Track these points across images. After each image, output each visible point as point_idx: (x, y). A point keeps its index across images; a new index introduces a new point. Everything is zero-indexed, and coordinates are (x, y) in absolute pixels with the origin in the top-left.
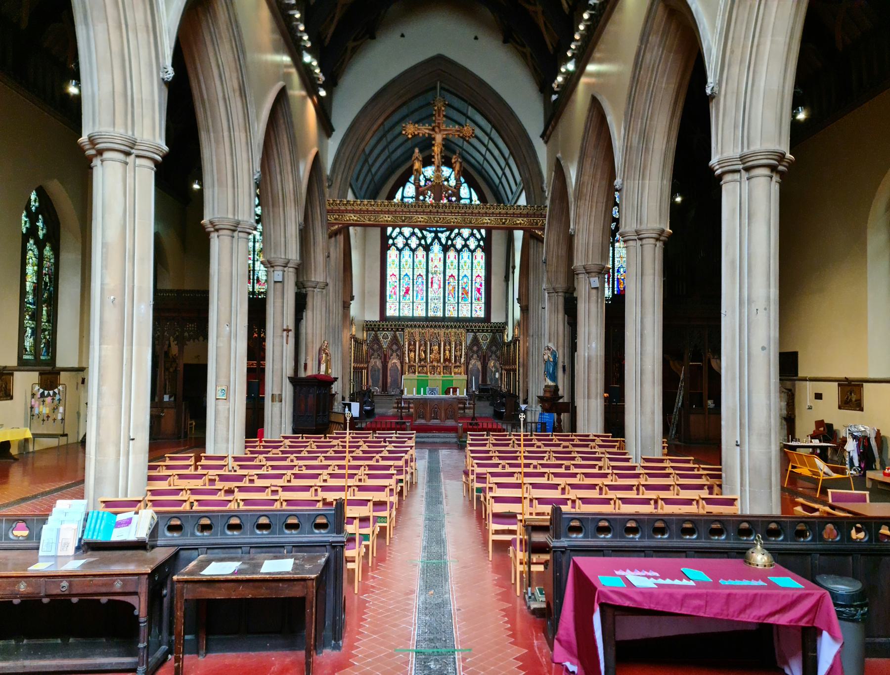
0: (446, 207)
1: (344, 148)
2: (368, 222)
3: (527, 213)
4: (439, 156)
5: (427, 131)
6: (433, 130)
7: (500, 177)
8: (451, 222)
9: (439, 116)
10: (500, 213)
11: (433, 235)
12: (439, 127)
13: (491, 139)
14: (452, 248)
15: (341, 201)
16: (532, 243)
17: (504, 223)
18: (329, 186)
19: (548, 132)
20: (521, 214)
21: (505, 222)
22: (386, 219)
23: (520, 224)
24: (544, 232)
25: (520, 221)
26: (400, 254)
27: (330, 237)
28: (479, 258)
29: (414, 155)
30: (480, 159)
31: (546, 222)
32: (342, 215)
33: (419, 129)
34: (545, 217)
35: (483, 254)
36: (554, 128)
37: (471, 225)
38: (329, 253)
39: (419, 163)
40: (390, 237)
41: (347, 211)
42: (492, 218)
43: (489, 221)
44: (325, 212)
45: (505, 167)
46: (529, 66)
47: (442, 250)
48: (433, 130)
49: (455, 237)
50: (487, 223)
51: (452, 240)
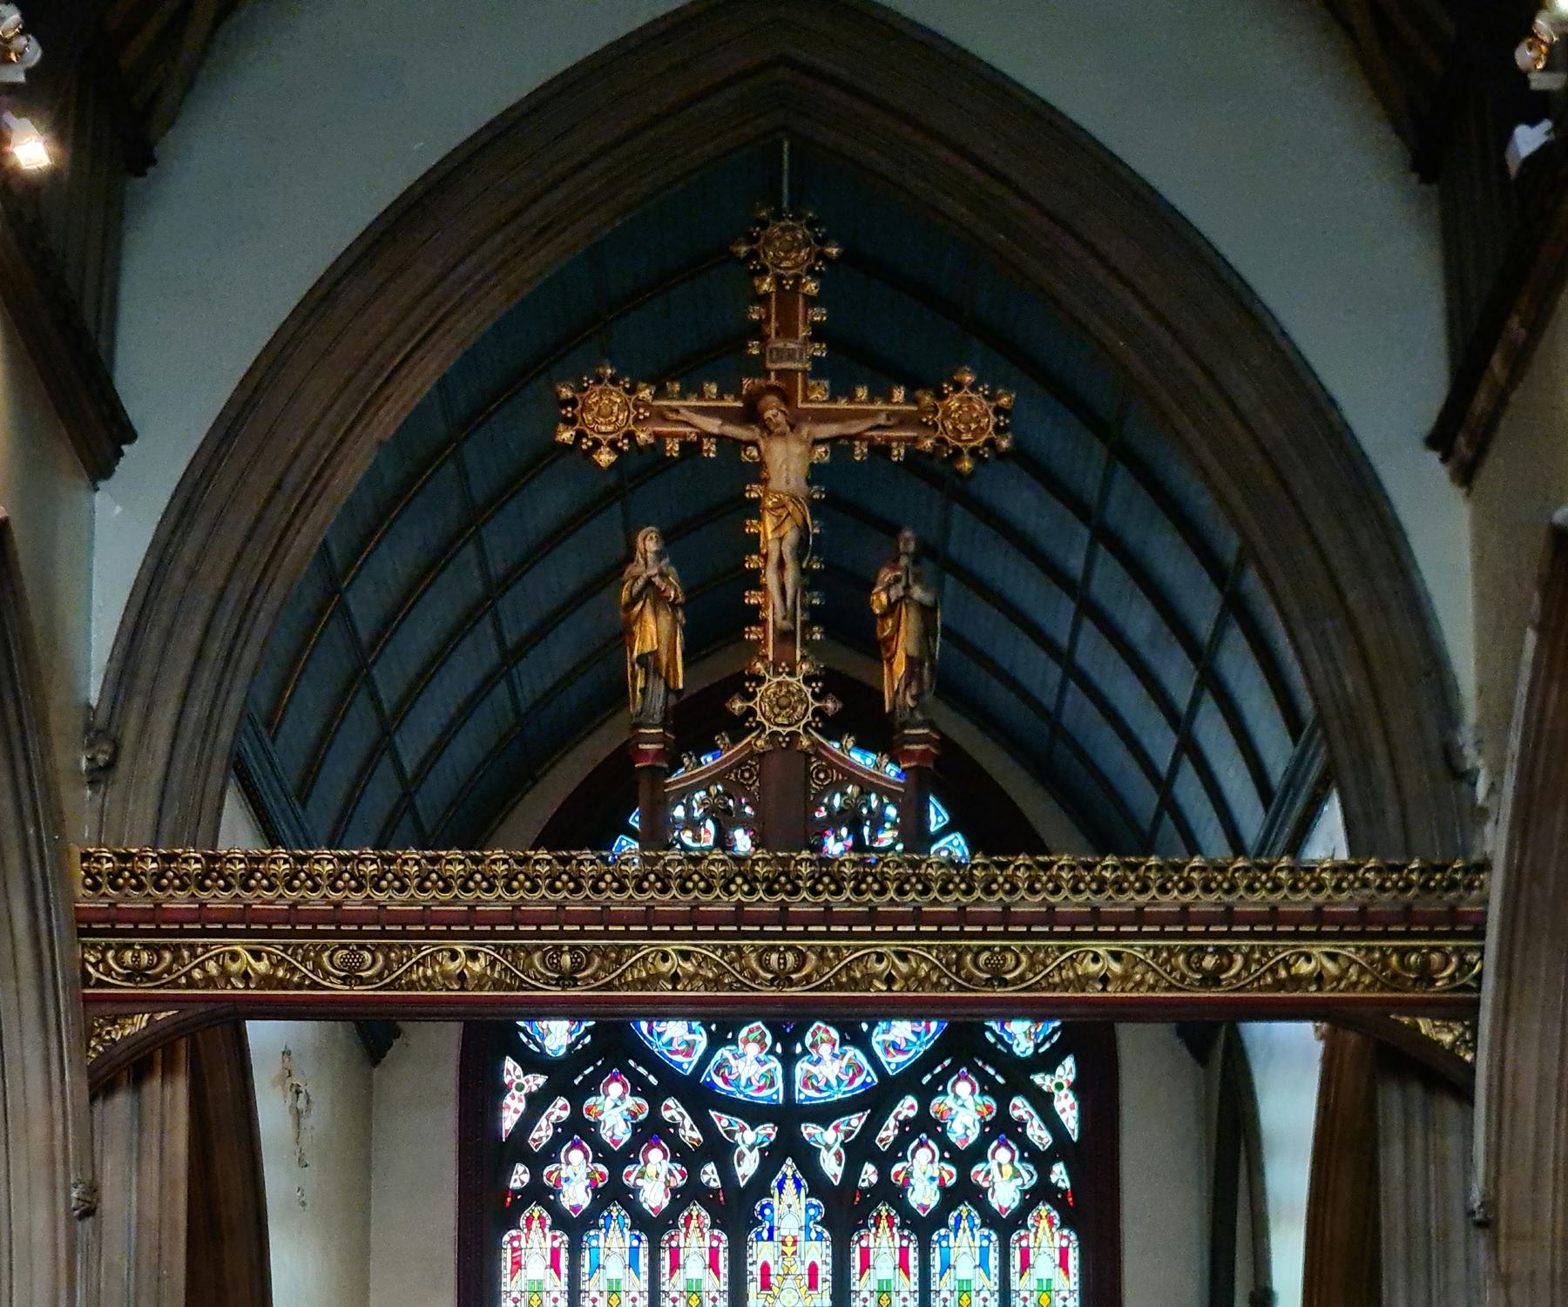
0: (838, 880)
1: (196, 537)
2: (344, 991)
3: (1363, 908)
4: (790, 575)
5: (713, 425)
6: (751, 414)
7: (1163, 767)
8: (869, 978)
9: (787, 331)
10: (1184, 915)
11: (768, 1131)
12: (787, 398)
13: (1106, 537)
14: (883, 1209)
15: (168, 859)
16: (1393, 1102)
17: (1211, 979)
18: (99, 775)
19: (1481, 402)
20: (1318, 915)
21: (1220, 969)
22: (453, 966)
23: (1319, 978)
24: (1474, 1029)
25: (1313, 960)
26: (575, 1250)
27: (102, 1085)
28: (1044, 1265)
29: (632, 569)
30: (1043, 675)
31: (1488, 965)
32: (176, 949)
33: (661, 416)
34: (1479, 934)
35: (1070, 1239)
36: (1520, 362)
37: (1000, 993)
38: (93, 1190)
39: (665, 620)
40: (517, 1148)
41: (208, 924)
42: (1137, 948)
43: (1116, 968)
44: (62, 931)
45: (1195, 702)
46: (1348, 27)
47: (824, 1223)
48: (751, 414)
49: (901, 1143)
50: (1105, 980)
51: (884, 1162)
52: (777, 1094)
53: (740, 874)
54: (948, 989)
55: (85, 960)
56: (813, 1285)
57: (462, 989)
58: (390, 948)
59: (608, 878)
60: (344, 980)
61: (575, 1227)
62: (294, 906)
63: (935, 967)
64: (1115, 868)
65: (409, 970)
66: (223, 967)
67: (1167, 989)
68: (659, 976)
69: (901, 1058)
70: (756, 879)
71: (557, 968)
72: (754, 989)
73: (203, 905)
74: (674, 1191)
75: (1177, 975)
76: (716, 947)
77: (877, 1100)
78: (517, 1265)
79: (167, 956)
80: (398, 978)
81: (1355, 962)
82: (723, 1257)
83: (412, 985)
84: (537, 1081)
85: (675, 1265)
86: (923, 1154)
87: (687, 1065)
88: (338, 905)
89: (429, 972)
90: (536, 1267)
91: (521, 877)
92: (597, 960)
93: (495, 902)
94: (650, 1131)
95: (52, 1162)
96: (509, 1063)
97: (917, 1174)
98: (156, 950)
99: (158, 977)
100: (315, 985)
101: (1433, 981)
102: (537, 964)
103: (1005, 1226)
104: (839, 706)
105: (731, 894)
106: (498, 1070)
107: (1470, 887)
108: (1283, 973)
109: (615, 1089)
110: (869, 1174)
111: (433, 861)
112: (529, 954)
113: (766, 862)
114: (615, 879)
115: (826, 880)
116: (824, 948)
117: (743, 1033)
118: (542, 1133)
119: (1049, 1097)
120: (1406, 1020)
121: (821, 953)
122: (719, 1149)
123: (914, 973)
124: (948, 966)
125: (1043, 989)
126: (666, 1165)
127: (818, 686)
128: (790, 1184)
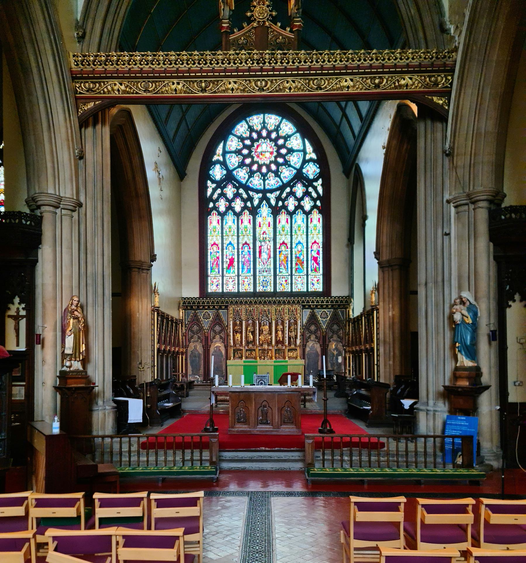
2: (145, 94)
3: (420, 64)
11: (260, 195)
14: (283, 210)
17: (377, 86)
21: (380, 83)
27: (83, 123)
34: (453, 71)
35: (320, 216)
40: (211, 199)
47: (272, 213)
49: (287, 197)
50: (348, 87)
51: (283, 201)
52: (262, 187)
53: (250, 58)
54: (306, 91)
55: (76, 86)
56: (269, 226)
57: (176, 93)
58: (157, 81)
59: (214, 60)
60: (145, 91)
61: (222, 215)
62: (130, 69)
63: (302, 85)
64: (352, 54)
65: (161, 88)
66: (112, 88)
67: (365, 90)
68: (228, 89)
69: (287, 179)
70: (254, 60)
71: (201, 87)
72: (254, 92)
73: (106, 69)
74: (242, 207)
75: (368, 85)
76: (243, 80)
77: (282, 188)
78: (211, 223)
79: (97, 85)
80: (159, 91)
81: (417, 80)
82: (252, 221)
83: (162, 93)
84: (214, 185)
85: (242, 222)
86: (291, 199)
87: (244, 182)
88: (142, 69)
89: (167, 89)
90: (215, 223)
91: (191, 60)
92: (212, 84)
93: (184, 67)
94: (237, 195)
95: (68, 140)
96: (209, 182)
97: (290, 203)
98: (94, 83)
99: (95, 91)
100: (137, 93)
101: (438, 85)
102: (195, 85)
103: (307, 213)
104: (276, 13)
105: (247, 64)
106: (206, 183)
107: (449, 57)
108: (397, 84)
109: (230, 187)
110: (280, 204)
111: (167, 55)
112: (193, 83)
113: (257, 54)
114: (216, 60)
115: (273, 59)
116: (272, 80)
117: (255, 175)
118: (215, 196)
119: (316, 187)
120: (430, 97)
121: (272, 82)
122: (251, 199)
123: (296, 87)
124: (306, 84)
125: (332, 91)
126: (240, 202)
127: (270, 8)
128: (265, 206)
